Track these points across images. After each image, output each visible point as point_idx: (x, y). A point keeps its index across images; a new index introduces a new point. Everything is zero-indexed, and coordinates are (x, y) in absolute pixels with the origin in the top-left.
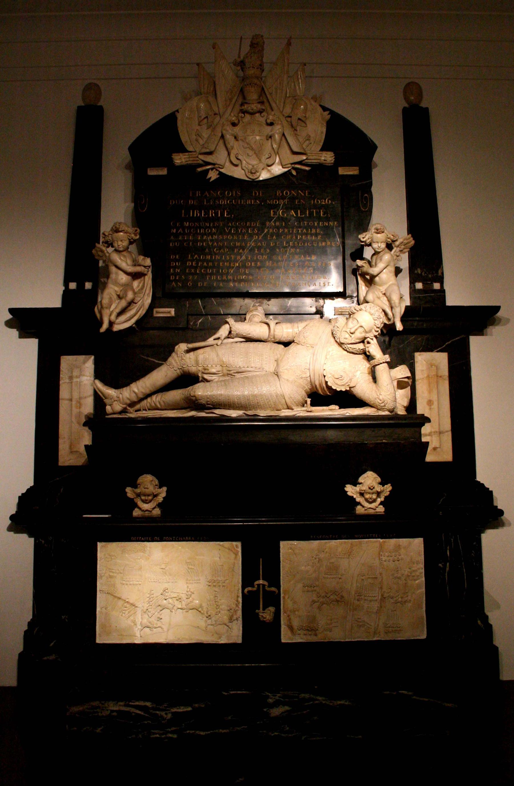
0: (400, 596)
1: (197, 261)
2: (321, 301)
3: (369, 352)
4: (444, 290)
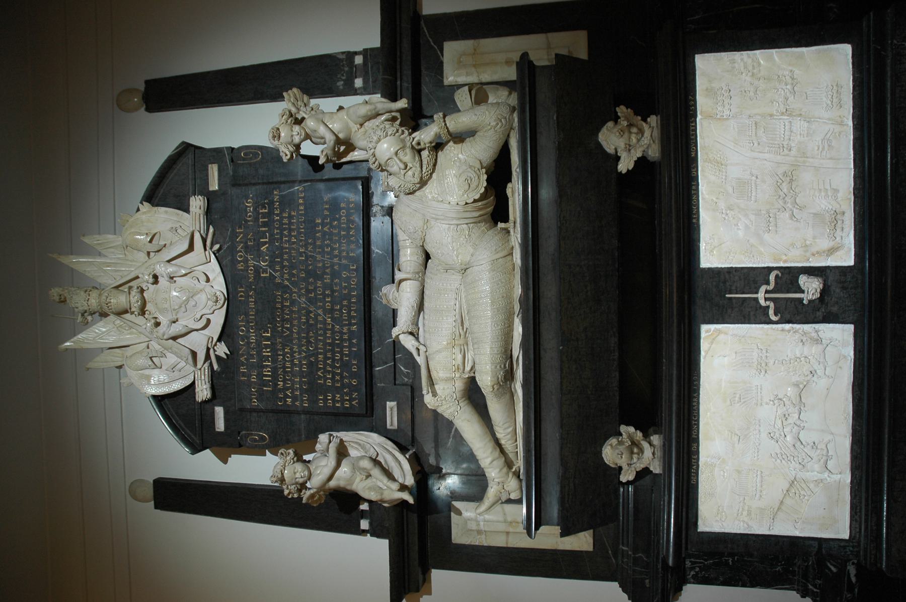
0: (784, 87)
1: (326, 371)
2: (375, 209)
3: (431, 143)
4: (364, 50)
